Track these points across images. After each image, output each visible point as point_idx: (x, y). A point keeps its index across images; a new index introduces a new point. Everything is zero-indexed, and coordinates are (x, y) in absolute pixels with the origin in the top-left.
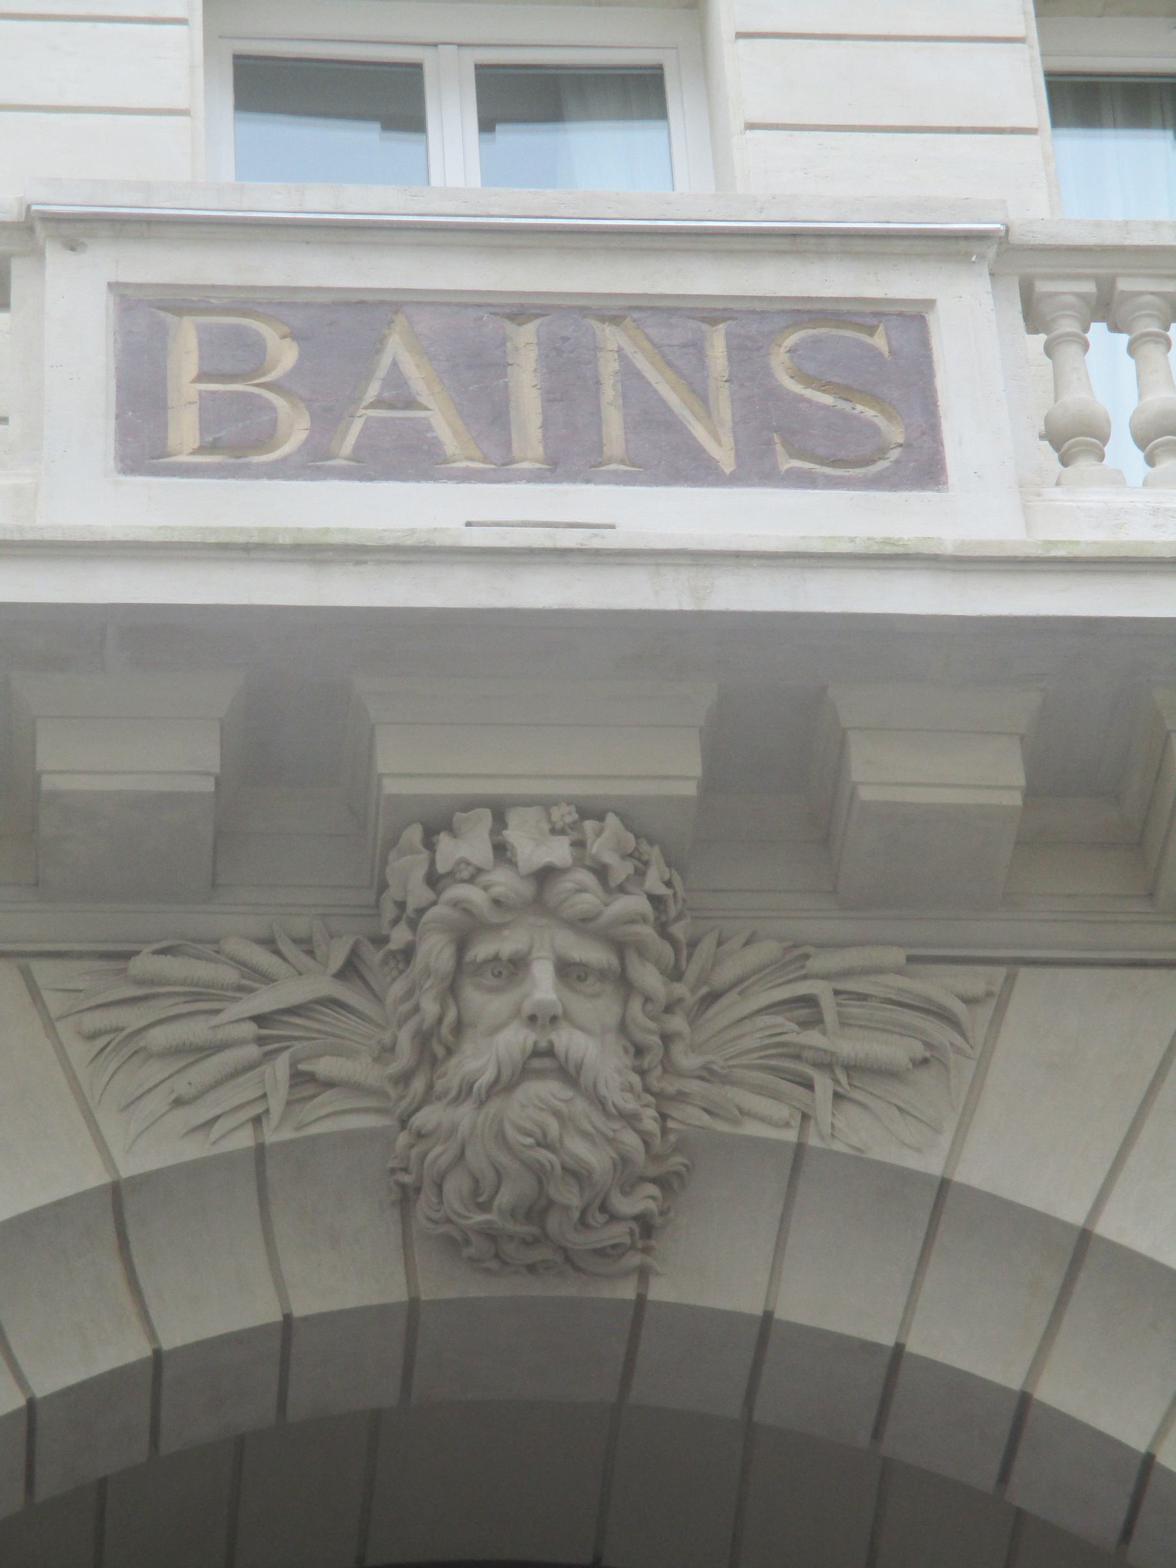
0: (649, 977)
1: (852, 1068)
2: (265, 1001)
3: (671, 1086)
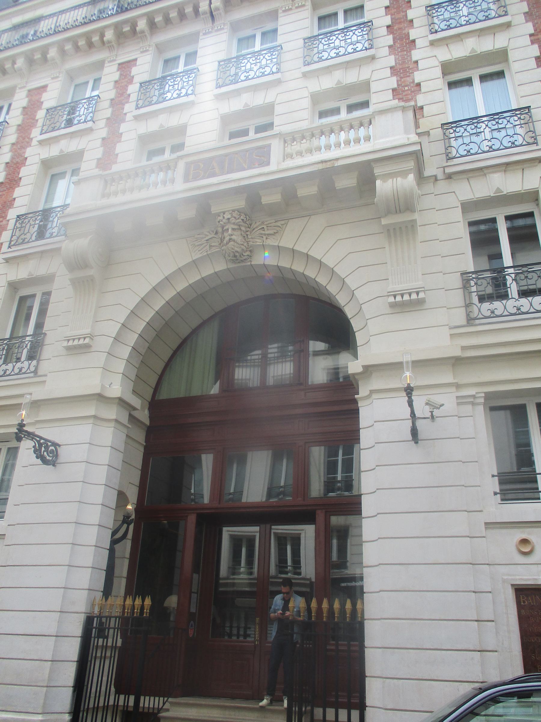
0: (243, 228)
1: (268, 235)
2: (207, 238)
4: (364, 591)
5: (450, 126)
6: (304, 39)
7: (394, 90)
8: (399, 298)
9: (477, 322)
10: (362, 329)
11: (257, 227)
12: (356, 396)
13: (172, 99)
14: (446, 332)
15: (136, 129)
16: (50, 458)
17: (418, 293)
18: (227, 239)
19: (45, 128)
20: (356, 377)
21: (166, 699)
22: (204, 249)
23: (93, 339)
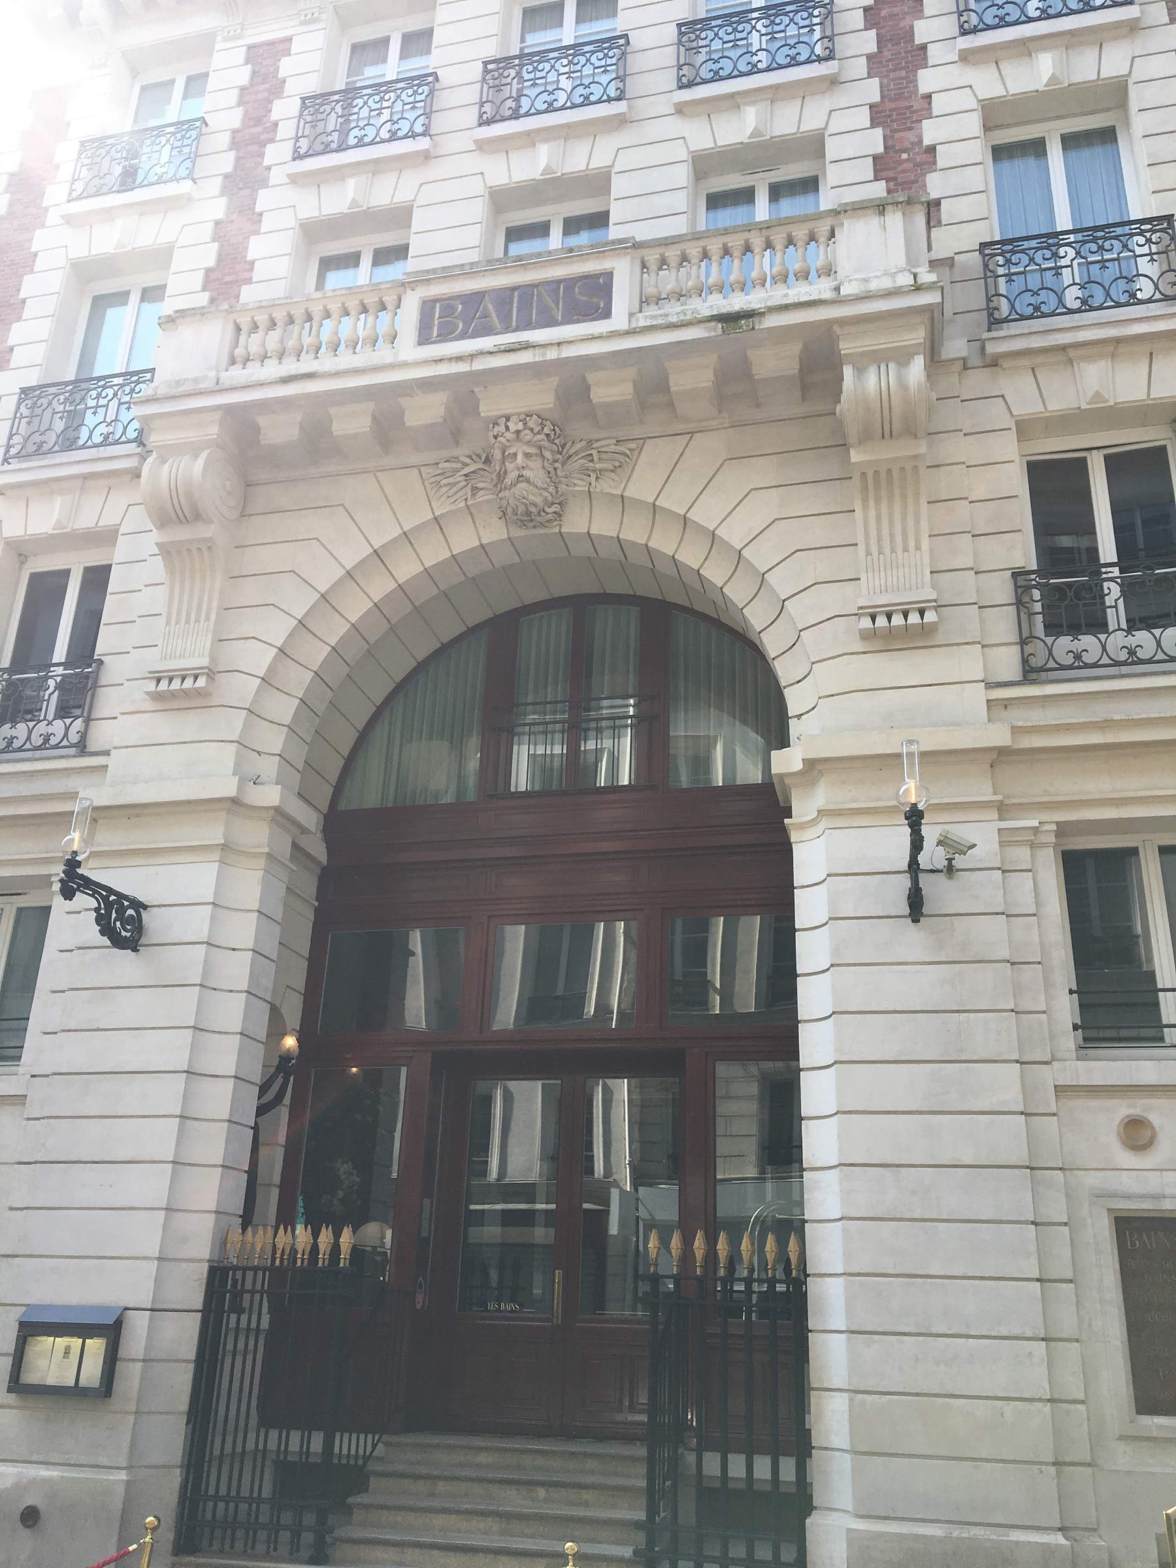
0: (548, 454)
1: (600, 470)
5: (998, 249)
6: (679, 26)
7: (876, 158)
8: (881, 621)
10: (799, 682)
11: (576, 453)
12: (787, 821)
14: (978, 696)
16: (128, 935)
17: (922, 612)
18: (512, 476)
19: (79, 187)
20: (787, 781)
22: (460, 494)
23: (213, 679)
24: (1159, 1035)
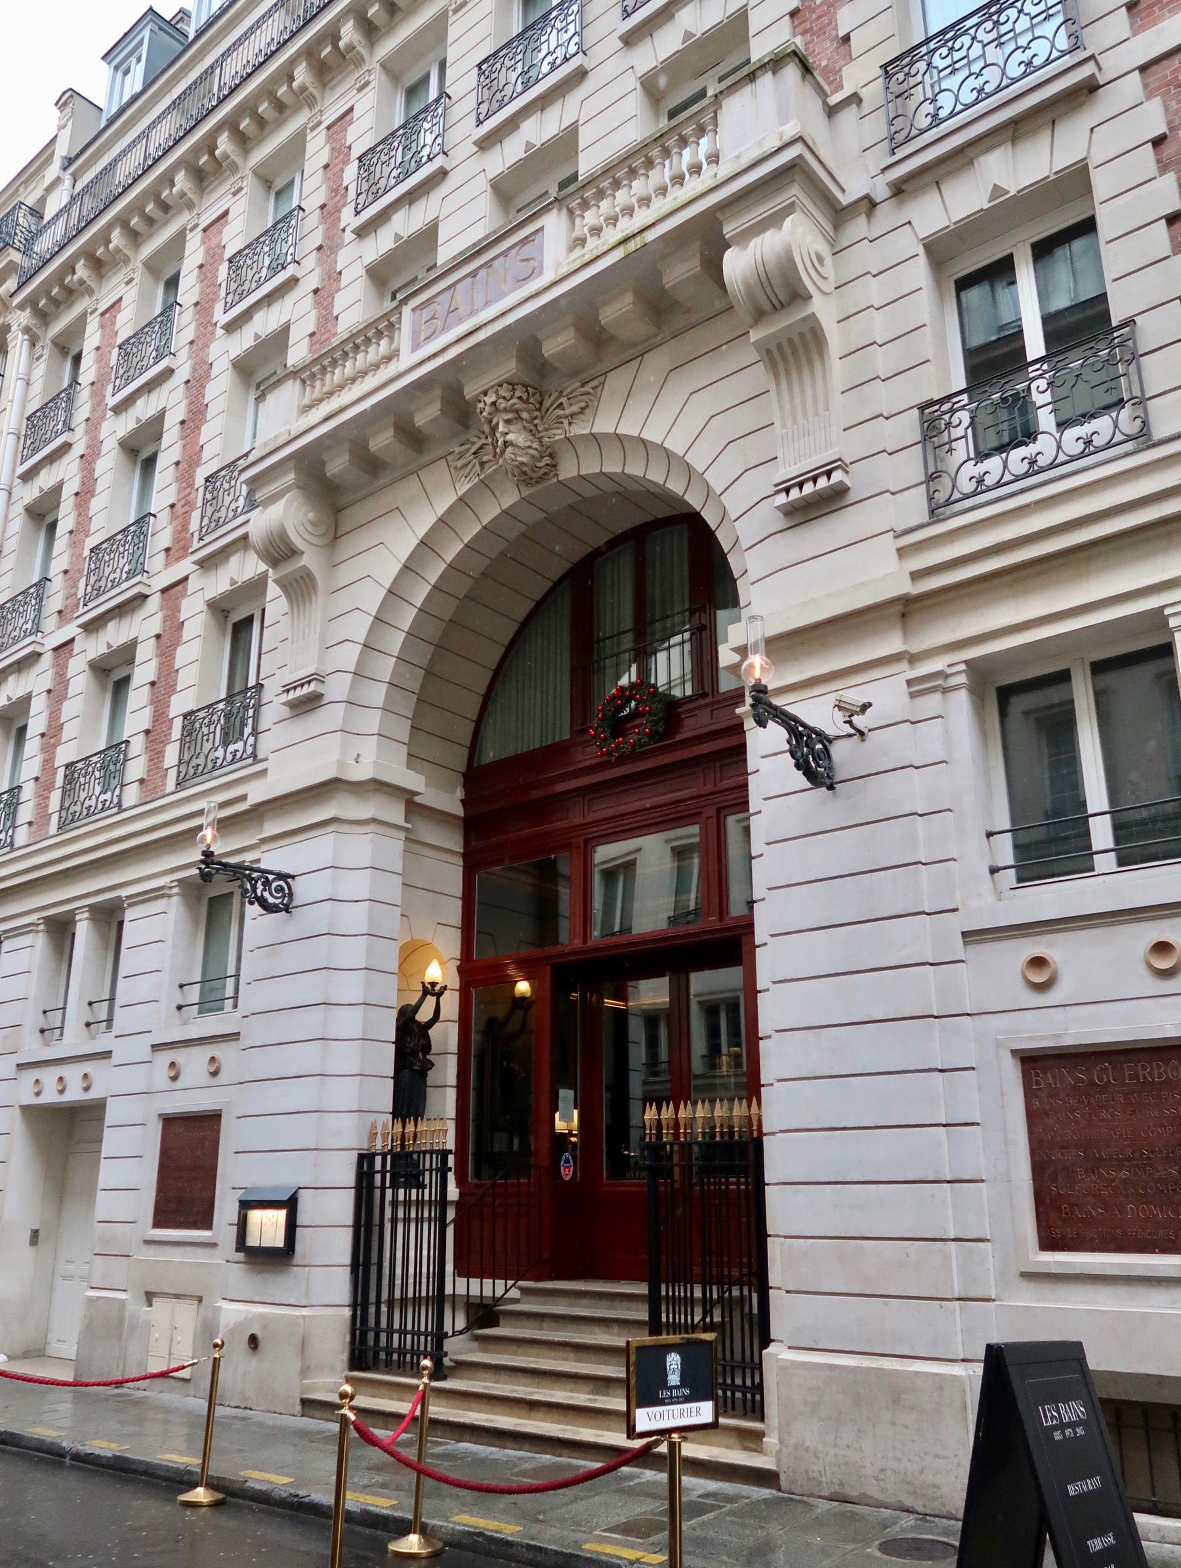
0: (525, 415)
2: (474, 449)
3: (539, 436)
4: (762, 1082)
9: (948, 511)
13: (542, 79)
14: (889, 544)
15: (632, 67)
21: (510, 1283)
24: (1089, 864)
